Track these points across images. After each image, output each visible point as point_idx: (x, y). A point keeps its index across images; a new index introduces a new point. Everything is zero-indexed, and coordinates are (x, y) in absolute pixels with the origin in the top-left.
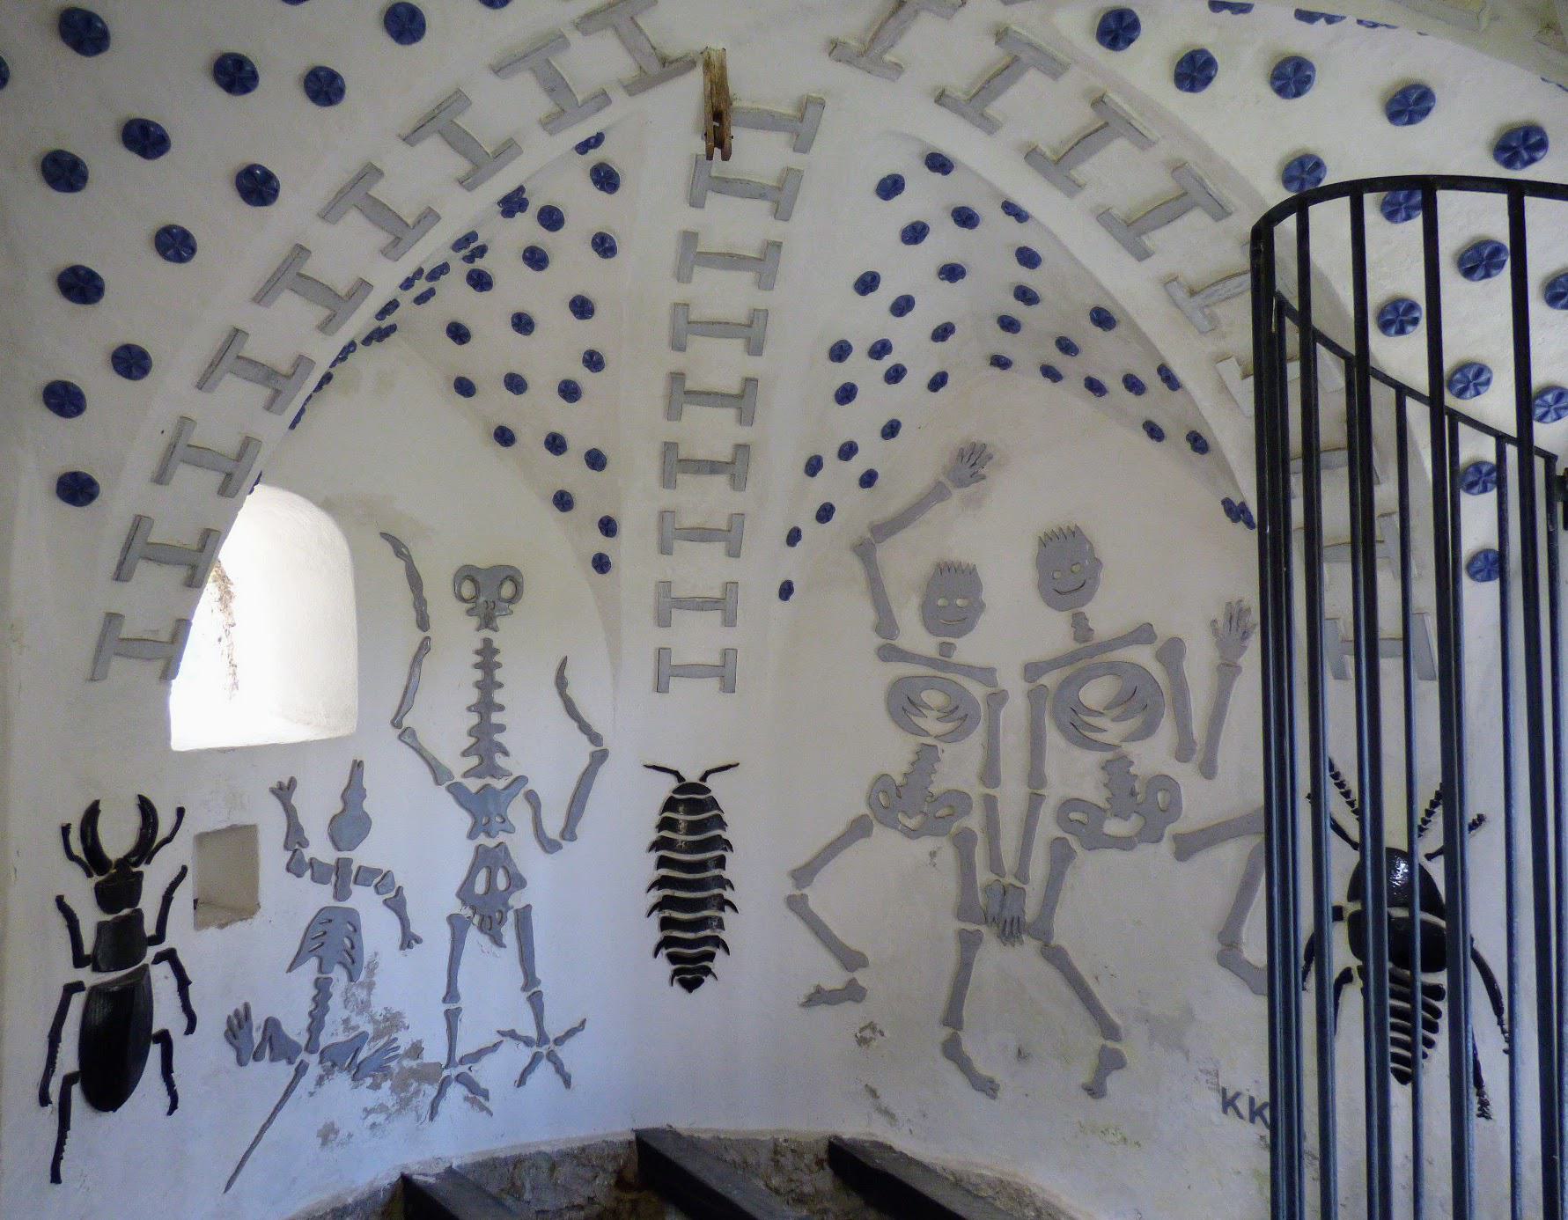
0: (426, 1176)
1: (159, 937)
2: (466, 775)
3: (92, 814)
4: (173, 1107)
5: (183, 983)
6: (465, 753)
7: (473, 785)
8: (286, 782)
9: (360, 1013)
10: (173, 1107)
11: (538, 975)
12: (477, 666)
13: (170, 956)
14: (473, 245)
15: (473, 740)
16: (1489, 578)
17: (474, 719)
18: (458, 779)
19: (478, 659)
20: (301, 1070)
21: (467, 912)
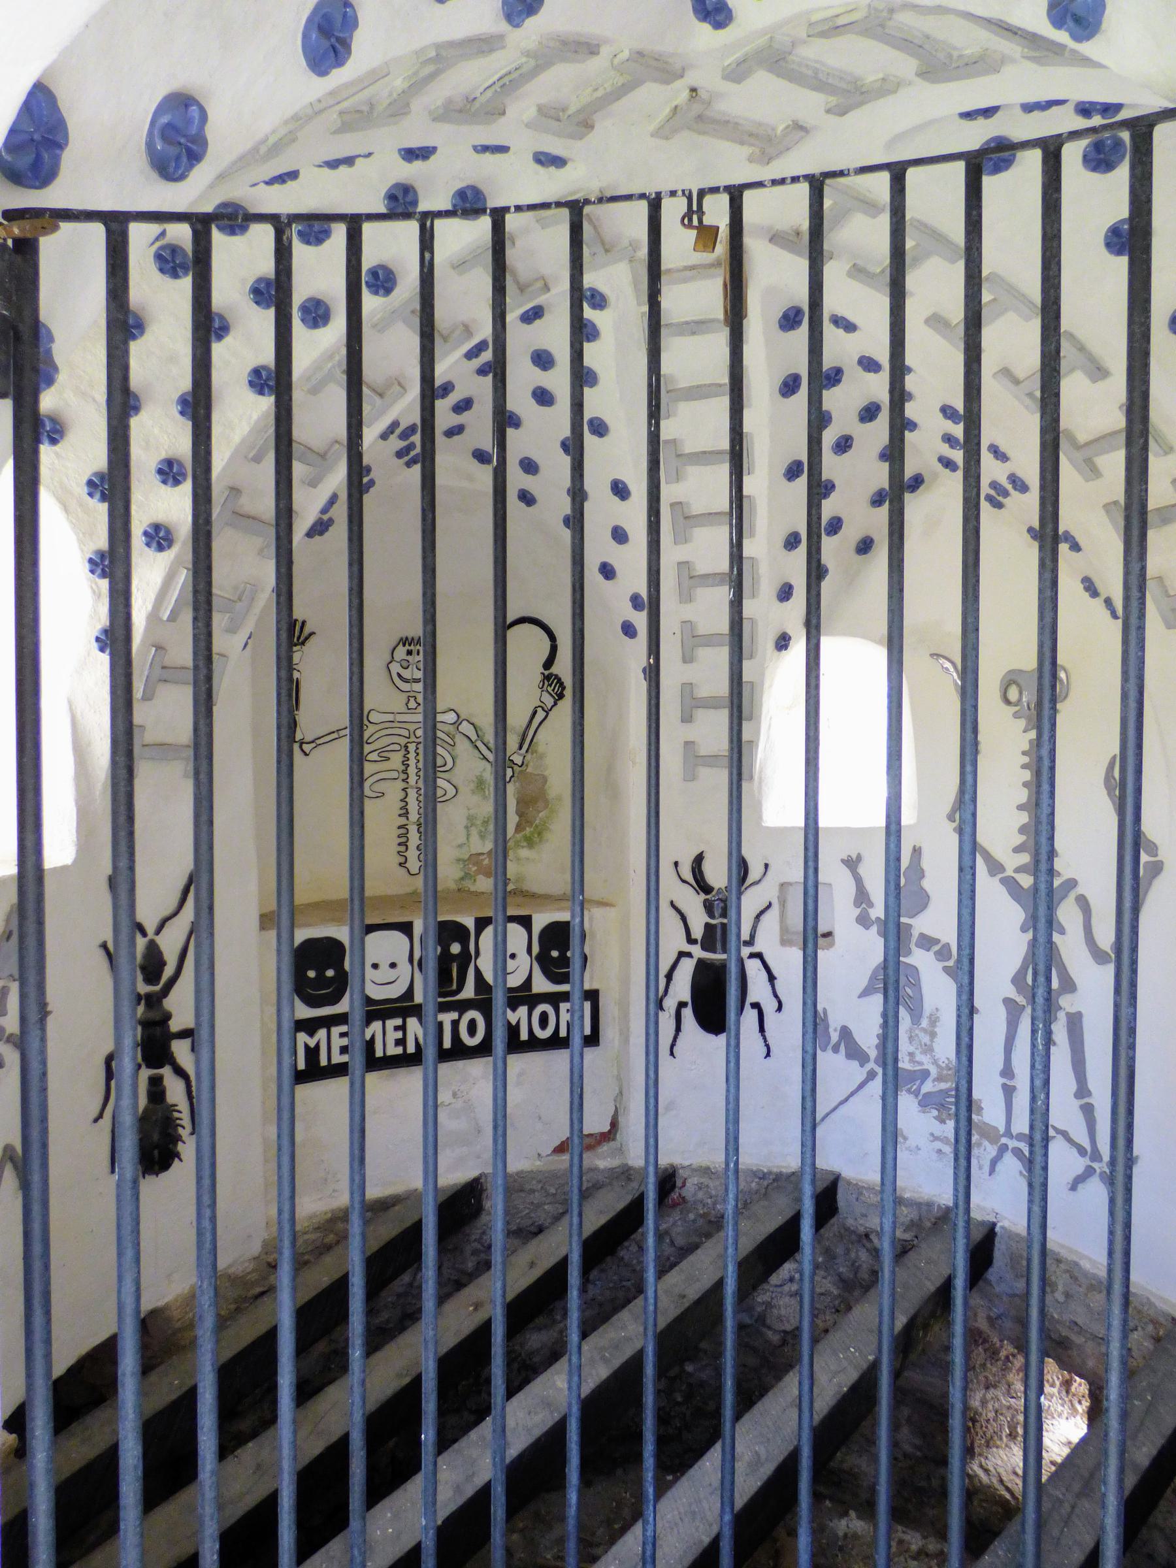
0: (843, 1175)
1: (750, 943)
2: (1017, 870)
3: (699, 860)
4: (768, 1055)
5: (772, 978)
6: (1017, 850)
8: (854, 857)
9: (924, 1052)
10: (768, 1055)
12: (1024, 767)
13: (759, 956)
14: (406, 459)
15: (1024, 838)
16: (268, 307)
18: (1009, 872)
19: (1026, 759)
20: (871, 1075)
21: (1021, 1000)
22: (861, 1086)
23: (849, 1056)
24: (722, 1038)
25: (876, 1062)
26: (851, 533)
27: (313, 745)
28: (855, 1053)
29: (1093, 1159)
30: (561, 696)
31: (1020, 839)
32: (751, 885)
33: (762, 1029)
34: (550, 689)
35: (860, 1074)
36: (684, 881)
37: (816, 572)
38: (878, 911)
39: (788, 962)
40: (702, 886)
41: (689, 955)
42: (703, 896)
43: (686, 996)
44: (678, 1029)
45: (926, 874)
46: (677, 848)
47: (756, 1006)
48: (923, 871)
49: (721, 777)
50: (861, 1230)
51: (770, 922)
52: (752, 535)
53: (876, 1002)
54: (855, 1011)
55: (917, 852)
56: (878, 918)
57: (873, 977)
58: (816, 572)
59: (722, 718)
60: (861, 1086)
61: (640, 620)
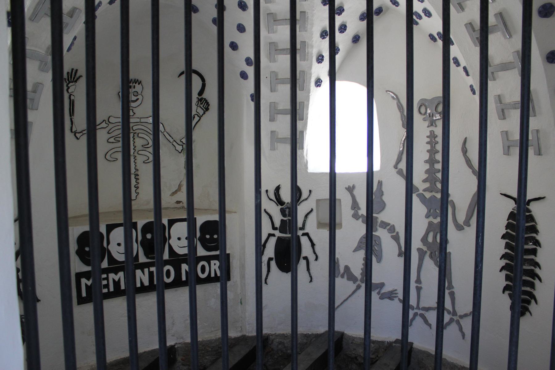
1: (303, 228)
2: (424, 190)
3: (278, 189)
4: (311, 281)
5: (313, 245)
7: (428, 195)
8: (351, 186)
10: (311, 281)
11: (453, 284)
12: (427, 143)
13: (307, 234)
15: (427, 175)
17: (427, 166)
18: (421, 191)
19: (428, 140)
20: (359, 287)
21: (425, 249)
22: (354, 292)
23: (349, 279)
24: (289, 274)
25: (362, 281)
26: (350, 32)
27: (82, 134)
28: (351, 277)
29: (453, 315)
30: (207, 109)
31: (425, 176)
32: (303, 201)
33: (308, 269)
34: (201, 106)
35: (353, 286)
36: (271, 200)
37: (333, 50)
38: (363, 211)
39: (321, 237)
40: (279, 201)
41: (273, 235)
42: (280, 207)
43: (272, 255)
44: (269, 271)
45: (384, 193)
46: (268, 185)
47: (306, 258)
48: (383, 192)
49: (287, 148)
50: (353, 356)
51: (312, 218)
52: (379, 260)
53: (362, 254)
54: (351, 258)
55: (380, 183)
56: (362, 215)
57: (360, 242)
58: (333, 50)
59: (288, 118)
60: (354, 292)
61: (250, 71)
